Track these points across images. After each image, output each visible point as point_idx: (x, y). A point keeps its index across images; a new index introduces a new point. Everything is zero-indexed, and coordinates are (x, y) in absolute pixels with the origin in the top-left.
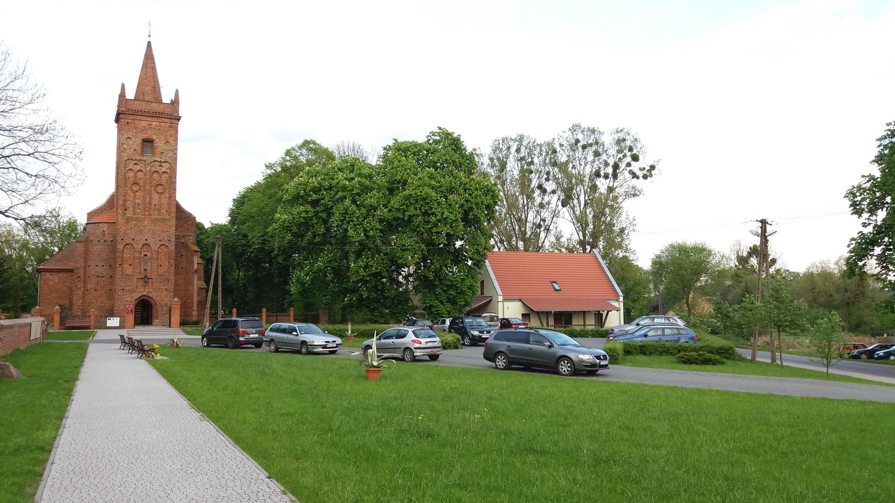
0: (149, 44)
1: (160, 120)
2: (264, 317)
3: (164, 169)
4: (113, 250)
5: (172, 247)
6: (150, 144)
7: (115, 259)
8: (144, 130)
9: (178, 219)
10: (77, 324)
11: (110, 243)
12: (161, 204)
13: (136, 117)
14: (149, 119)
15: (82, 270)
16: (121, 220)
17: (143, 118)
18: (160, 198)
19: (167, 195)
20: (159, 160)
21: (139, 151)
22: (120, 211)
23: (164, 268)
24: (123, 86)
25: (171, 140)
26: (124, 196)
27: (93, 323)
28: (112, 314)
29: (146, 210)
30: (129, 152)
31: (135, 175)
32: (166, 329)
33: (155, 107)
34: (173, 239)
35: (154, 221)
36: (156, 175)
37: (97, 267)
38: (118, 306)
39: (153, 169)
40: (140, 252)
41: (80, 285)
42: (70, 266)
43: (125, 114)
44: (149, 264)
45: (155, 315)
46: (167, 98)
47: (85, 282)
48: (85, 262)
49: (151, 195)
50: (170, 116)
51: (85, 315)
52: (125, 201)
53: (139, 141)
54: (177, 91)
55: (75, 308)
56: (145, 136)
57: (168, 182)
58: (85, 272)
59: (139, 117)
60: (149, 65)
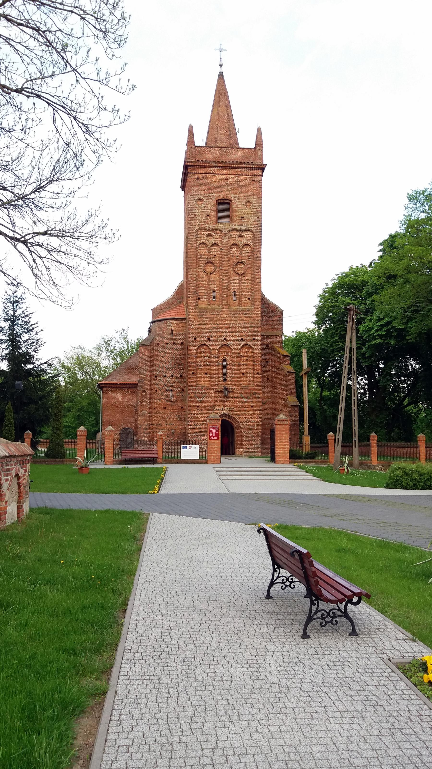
0: (221, 75)
1: (239, 172)
2: (374, 450)
3: (245, 241)
4: (184, 347)
5: (258, 349)
6: (225, 207)
7: (186, 366)
8: (218, 187)
9: (264, 313)
10: (143, 456)
11: (179, 345)
12: (242, 290)
13: (208, 170)
14: (225, 171)
15: (147, 382)
16: (193, 313)
17: (216, 170)
18: (240, 281)
19: (249, 276)
22: (191, 300)
24: (191, 128)
25: (254, 200)
27: (160, 453)
28: (184, 439)
29: (223, 299)
32: (261, 464)
33: (232, 155)
34: (259, 337)
35: (234, 313)
36: (235, 249)
37: (165, 379)
38: (193, 429)
39: (231, 242)
40: (218, 356)
41: (146, 401)
42: (134, 380)
43: (194, 168)
44: (229, 372)
45: (237, 441)
46: (246, 140)
47: (151, 398)
48: (151, 372)
49: (229, 277)
50: (253, 166)
51: (152, 442)
52: (197, 287)
53: (213, 203)
54: (259, 131)
55: (141, 431)
57: (249, 262)
58: (151, 385)
59: (212, 170)
60: (222, 103)
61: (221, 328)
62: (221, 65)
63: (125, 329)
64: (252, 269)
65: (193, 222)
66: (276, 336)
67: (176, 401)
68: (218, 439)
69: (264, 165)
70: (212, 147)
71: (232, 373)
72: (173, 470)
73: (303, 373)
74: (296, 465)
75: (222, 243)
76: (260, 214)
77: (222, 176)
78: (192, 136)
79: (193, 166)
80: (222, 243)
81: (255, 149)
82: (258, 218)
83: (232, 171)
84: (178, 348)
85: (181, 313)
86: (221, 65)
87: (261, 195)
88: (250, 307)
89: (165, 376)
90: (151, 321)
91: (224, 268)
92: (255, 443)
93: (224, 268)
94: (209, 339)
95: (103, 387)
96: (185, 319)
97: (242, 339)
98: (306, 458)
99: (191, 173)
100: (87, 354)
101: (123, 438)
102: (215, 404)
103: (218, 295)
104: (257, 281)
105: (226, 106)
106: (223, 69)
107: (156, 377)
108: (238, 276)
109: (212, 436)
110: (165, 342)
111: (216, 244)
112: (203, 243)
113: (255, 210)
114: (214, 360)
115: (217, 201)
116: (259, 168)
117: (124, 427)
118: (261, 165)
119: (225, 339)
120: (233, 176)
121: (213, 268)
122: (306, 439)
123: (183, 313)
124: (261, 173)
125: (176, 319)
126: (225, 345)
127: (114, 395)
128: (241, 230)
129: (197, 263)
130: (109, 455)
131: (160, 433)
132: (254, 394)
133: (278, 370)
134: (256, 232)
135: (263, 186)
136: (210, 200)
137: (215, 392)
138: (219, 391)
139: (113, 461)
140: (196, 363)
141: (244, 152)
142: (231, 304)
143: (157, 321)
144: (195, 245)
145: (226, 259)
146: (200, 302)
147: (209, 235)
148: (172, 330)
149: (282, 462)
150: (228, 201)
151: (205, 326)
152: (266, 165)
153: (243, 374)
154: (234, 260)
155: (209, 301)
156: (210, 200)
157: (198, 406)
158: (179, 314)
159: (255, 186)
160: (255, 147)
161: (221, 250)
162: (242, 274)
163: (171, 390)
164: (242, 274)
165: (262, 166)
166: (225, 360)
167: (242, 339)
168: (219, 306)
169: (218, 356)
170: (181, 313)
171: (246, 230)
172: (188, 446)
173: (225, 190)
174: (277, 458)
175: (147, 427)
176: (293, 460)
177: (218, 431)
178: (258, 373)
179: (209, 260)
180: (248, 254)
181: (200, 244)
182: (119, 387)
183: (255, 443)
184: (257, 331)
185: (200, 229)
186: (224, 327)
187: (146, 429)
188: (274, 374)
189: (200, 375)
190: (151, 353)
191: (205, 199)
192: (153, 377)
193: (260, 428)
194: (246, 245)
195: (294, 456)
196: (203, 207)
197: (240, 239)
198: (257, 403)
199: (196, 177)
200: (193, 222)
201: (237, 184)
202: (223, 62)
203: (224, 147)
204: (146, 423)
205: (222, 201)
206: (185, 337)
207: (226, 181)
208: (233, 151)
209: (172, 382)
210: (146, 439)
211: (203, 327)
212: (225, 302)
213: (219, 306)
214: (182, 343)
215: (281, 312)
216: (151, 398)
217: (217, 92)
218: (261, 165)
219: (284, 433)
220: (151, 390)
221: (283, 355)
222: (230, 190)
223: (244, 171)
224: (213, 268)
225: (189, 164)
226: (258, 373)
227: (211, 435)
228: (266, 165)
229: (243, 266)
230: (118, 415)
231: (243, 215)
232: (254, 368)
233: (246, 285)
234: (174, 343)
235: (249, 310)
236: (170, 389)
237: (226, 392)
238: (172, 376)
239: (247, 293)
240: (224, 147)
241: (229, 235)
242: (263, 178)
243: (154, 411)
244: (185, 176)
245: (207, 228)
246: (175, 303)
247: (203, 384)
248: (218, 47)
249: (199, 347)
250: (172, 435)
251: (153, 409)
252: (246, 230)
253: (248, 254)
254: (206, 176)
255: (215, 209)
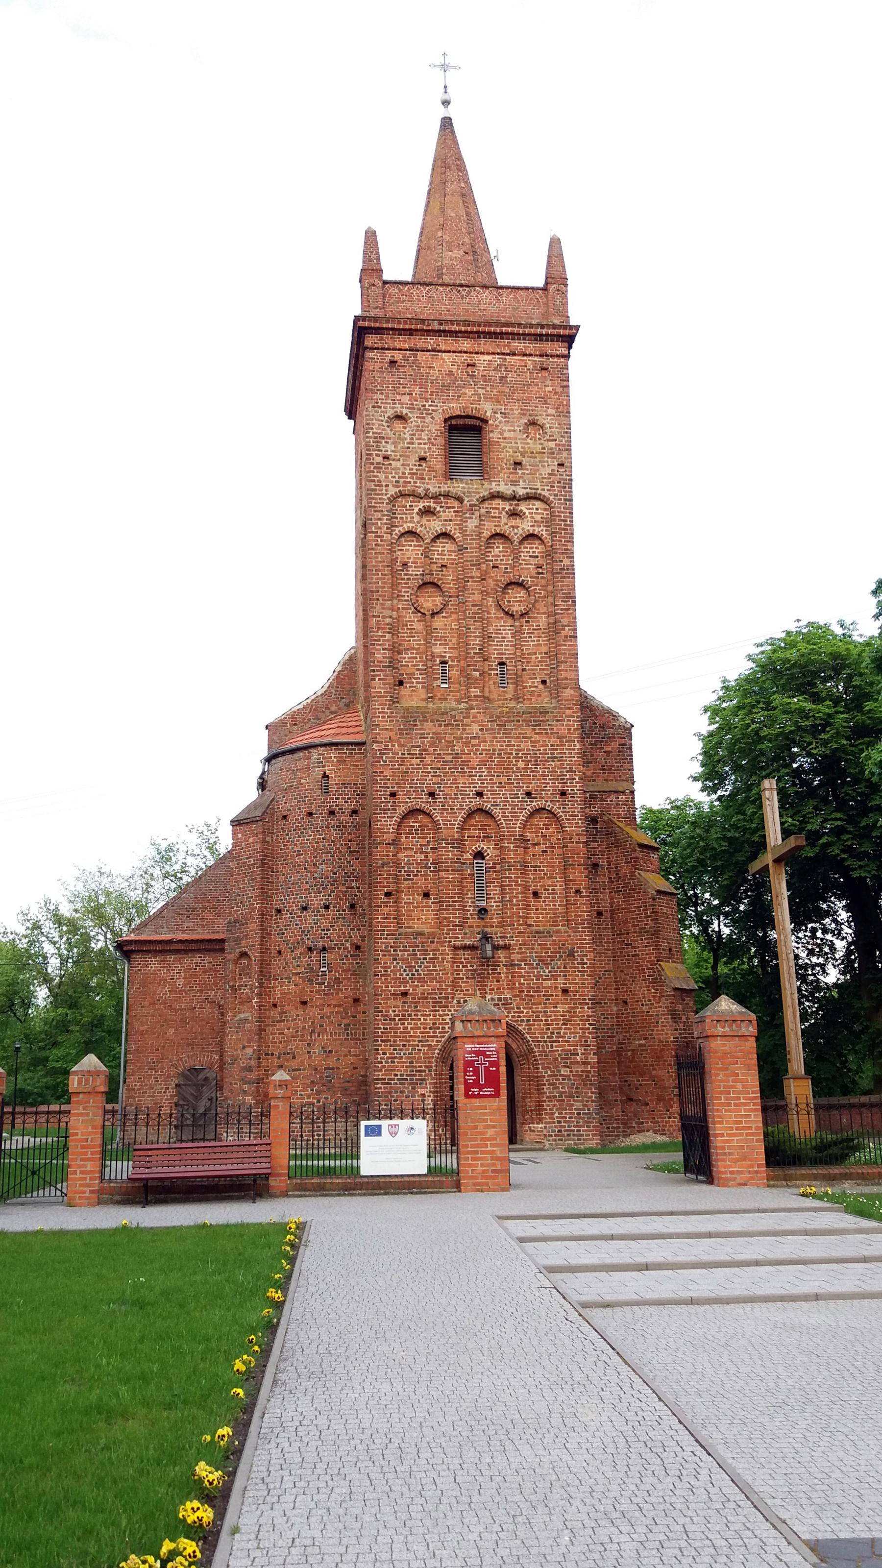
0: (447, 124)
1: (504, 345)
3: (526, 526)
5: (575, 825)
6: (468, 439)
7: (368, 877)
8: (448, 385)
11: (346, 818)
12: (521, 658)
13: (420, 341)
15: (253, 927)
17: (443, 343)
18: (517, 633)
19: (542, 621)
20: (505, 489)
21: (438, 462)
22: (379, 687)
23: (542, 914)
24: (371, 238)
26: (394, 630)
27: (282, 1156)
28: (362, 1100)
30: (400, 472)
31: (427, 554)
33: (483, 306)
34: (575, 788)
35: (502, 721)
36: (498, 548)
37: (308, 915)
38: (390, 1065)
40: (458, 844)
41: (249, 985)
42: (217, 929)
44: (494, 890)
47: (264, 974)
48: (265, 896)
49: (485, 622)
52: (396, 650)
53: (435, 426)
54: (555, 246)
56: (455, 408)
58: (265, 934)
59: (431, 342)
60: (451, 187)
61: (466, 763)
62: (446, 103)
63: (212, 822)
64: (550, 599)
65: (382, 476)
66: (617, 792)
67: (337, 980)
68: (497, 1095)
69: (571, 327)
70: (430, 284)
71: (503, 894)
72: (324, 1218)
73: (768, 858)
74: (832, 1198)
75: (463, 531)
76: (565, 454)
77: (456, 369)
78: (373, 256)
79: (378, 331)
80: (463, 531)
81: (545, 289)
82: (561, 465)
83: (484, 344)
84: (341, 827)
85: (351, 730)
86: (446, 103)
87: (568, 405)
88: (545, 701)
89: (305, 908)
90: (265, 754)
91: (472, 598)
92: (578, 1105)
93: (472, 598)
94: (432, 794)
95: (132, 951)
96: (363, 744)
97: (528, 794)
98: (816, 1162)
99: (372, 349)
100: (119, 884)
101: (184, 1099)
102: (455, 985)
103: (455, 673)
104: (563, 633)
105: (463, 195)
106: (451, 111)
107: (279, 911)
108: (510, 621)
109: (476, 1083)
110: (305, 809)
111: (445, 535)
112: (410, 533)
113: (552, 444)
114: (449, 854)
115: (446, 420)
116: (559, 338)
117: (187, 1065)
118: (565, 327)
119: (480, 794)
120: (489, 357)
121: (439, 600)
122: (799, 1090)
123: (358, 729)
124: (564, 351)
125: (336, 744)
126: (480, 810)
127: (163, 973)
128: (514, 498)
129: (394, 586)
130: (82, 1166)
131: (281, 1076)
132: (571, 954)
133: (630, 889)
134: (556, 503)
135: (571, 383)
136: (428, 419)
137: (456, 948)
138: (465, 948)
139: (101, 1191)
140: (397, 865)
141: (515, 298)
142: (494, 696)
143: (283, 754)
144: (387, 537)
145: (475, 573)
146: (405, 691)
147: (427, 512)
148: (325, 776)
149: (739, 1178)
150: (478, 423)
151: (421, 757)
152: (577, 328)
153: (535, 894)
154: (499, 577)
155: (429, 688)
156: (428, 419)
157: (405, 994)
158: (344, 730)
159: (548, 382)
160: (547, 283)
161: (461, 549)
162: (522, 615)
163: (324, 949)
164: (522, 615)
165: (567, 332)
166: (479, 855)
167: (528, 794)
168: (459, 701)
169: (458, 844)
170: (351, 730)
171: (528, 498)
172: (385, 1123)
173: (469, 392)
174: (722, 1165)
175: (253, 1063)
176: (779, 1172)
177: (496, 1064)
178: (578, 891)
179: (428, 578)
180: (535, 561)
181: (402, 535)
182: (177, 952)
183: (578, 1105)
184: (571, 771)
185: (402, 495)
186: (475, 760)
187: (249, 1069)
188: (619, 900)
189: (410, 899)
190: (264, 842)
191: (413, 417)
192: (269, 913)
193: (593, 1059)
194: (531, 536)
195: (783, 1158)
196: (407, 436)
197: (513, 522)
198: (580, 980)
199: (388, 359)
200: (382, 476)
201: (501, 378)
202: (452, 95)
203: (462, 286)
204: (249, 1051)
205: (460, 422)
206: (363, 795)
207: (470, 369)
208: (486, 294)
209: (325, 923)
210: (249, 1099)
211: (415, 761)
212: (475, 691)
213: (459, 701)
214: (355, 812)
215: (627, 730)
216: (264, 974)
217: (439, 163)
218: (565, 327)
219: (739, 1068)
220: (264, 951)
221: (642, 846)
222: (481, 391)
223: (518, 345)
224: (439, 600)
225: (366, 324)
226: (578, 891)
227: (471, 1079)
228: (577, 328)
229: (523, 593)
230: (172, 1031)
231: (519, 458)
232: (565, 875)
233: (536, 644)
234: (332, 813)
235: (545, 712)
236: (321, 944)
237: (489, 947)
238: (327, 907)
239: (537, 668)
240: (462, 286)
241: (483, 511)
242: (571, 362)
243: (274, 1013)
244: (356, 367)
245: (420, 491)
246: (334, 708)
247: (418, 927)
248: (440, 60)
249: (405, 817)
250: (327, 1084)
251: (268, 1006)
252: (528, 498)
253: (535, 561)
254: (415, 356)
255: (441, 441)
